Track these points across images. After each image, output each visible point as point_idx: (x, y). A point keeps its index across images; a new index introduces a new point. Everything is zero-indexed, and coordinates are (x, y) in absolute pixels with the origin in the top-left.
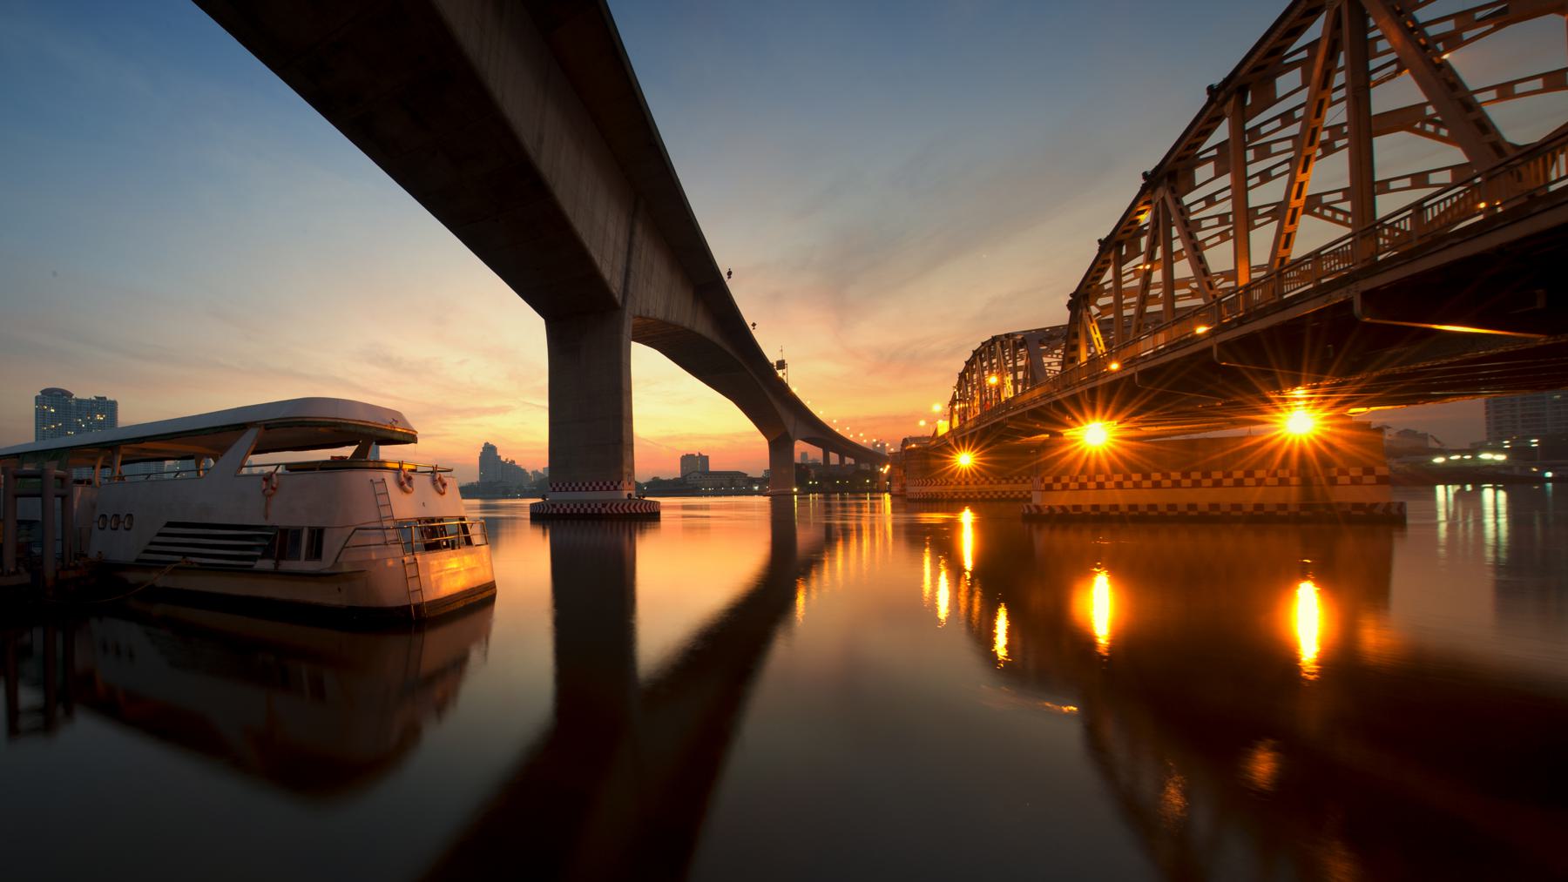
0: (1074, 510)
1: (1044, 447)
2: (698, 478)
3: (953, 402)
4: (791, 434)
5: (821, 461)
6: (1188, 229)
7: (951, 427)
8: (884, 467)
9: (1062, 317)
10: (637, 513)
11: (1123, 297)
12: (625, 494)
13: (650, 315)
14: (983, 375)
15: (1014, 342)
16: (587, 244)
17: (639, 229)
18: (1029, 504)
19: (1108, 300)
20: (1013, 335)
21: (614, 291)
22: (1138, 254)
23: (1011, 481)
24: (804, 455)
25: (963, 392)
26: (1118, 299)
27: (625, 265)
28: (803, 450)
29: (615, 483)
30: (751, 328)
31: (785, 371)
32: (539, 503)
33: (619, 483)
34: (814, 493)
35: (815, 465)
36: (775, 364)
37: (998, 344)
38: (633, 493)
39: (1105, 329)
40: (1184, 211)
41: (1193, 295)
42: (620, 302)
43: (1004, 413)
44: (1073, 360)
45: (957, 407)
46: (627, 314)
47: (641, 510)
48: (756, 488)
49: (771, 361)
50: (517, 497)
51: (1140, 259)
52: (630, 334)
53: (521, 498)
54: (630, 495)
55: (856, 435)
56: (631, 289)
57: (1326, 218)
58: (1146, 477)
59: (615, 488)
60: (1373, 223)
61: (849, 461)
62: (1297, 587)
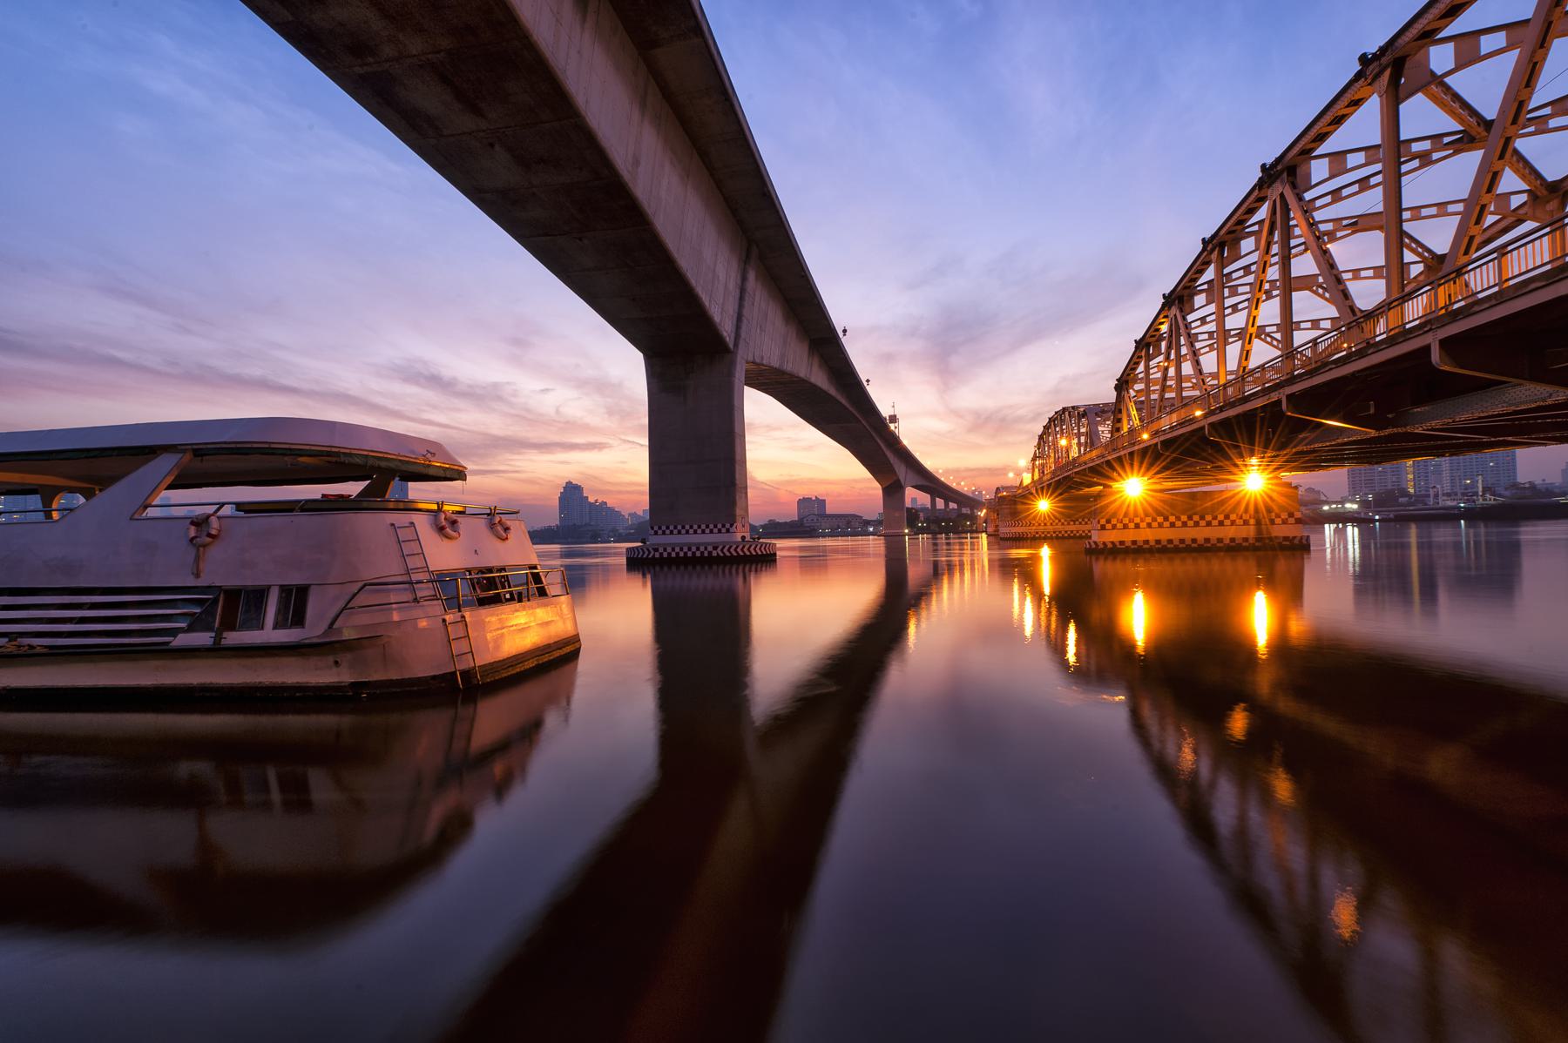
1: (1098, 496)
3: (1034, 459)
5: (929, 506)
6: (1190, 340)
7: (1033, 479)
9: (1110, 396)
15: (1078, 413)
16: (693, 282)
17: (751, 276)
20: (1078, 407)
21: (725, 334)
22: (1160, 354)
23: (1077, 523)
24: (914, 500)
26: (1147, 386)
27: (737, 310)
28: (914, 497)
29: (728, 526)
30: (865, 384)
31: (896, 425)
32: (637, 548)
33: (731, 526)
34: (923, 534)
35: (924, 509)
37: (1067, 413)
39: (1140, 406)
40: (1188, 326)
42: (731, 346)
44: (1118, 430)
45: (1037, 463)
48: (871, 529)
49: (884, 415)
51: (1161, 358)
52: (743, 379)
53: (614, 542)
54: (743, 538)
56: (743, 335)
57: (1267, 343)
58: (1166, 519)
59: (728, 531)
61: (953, 505)
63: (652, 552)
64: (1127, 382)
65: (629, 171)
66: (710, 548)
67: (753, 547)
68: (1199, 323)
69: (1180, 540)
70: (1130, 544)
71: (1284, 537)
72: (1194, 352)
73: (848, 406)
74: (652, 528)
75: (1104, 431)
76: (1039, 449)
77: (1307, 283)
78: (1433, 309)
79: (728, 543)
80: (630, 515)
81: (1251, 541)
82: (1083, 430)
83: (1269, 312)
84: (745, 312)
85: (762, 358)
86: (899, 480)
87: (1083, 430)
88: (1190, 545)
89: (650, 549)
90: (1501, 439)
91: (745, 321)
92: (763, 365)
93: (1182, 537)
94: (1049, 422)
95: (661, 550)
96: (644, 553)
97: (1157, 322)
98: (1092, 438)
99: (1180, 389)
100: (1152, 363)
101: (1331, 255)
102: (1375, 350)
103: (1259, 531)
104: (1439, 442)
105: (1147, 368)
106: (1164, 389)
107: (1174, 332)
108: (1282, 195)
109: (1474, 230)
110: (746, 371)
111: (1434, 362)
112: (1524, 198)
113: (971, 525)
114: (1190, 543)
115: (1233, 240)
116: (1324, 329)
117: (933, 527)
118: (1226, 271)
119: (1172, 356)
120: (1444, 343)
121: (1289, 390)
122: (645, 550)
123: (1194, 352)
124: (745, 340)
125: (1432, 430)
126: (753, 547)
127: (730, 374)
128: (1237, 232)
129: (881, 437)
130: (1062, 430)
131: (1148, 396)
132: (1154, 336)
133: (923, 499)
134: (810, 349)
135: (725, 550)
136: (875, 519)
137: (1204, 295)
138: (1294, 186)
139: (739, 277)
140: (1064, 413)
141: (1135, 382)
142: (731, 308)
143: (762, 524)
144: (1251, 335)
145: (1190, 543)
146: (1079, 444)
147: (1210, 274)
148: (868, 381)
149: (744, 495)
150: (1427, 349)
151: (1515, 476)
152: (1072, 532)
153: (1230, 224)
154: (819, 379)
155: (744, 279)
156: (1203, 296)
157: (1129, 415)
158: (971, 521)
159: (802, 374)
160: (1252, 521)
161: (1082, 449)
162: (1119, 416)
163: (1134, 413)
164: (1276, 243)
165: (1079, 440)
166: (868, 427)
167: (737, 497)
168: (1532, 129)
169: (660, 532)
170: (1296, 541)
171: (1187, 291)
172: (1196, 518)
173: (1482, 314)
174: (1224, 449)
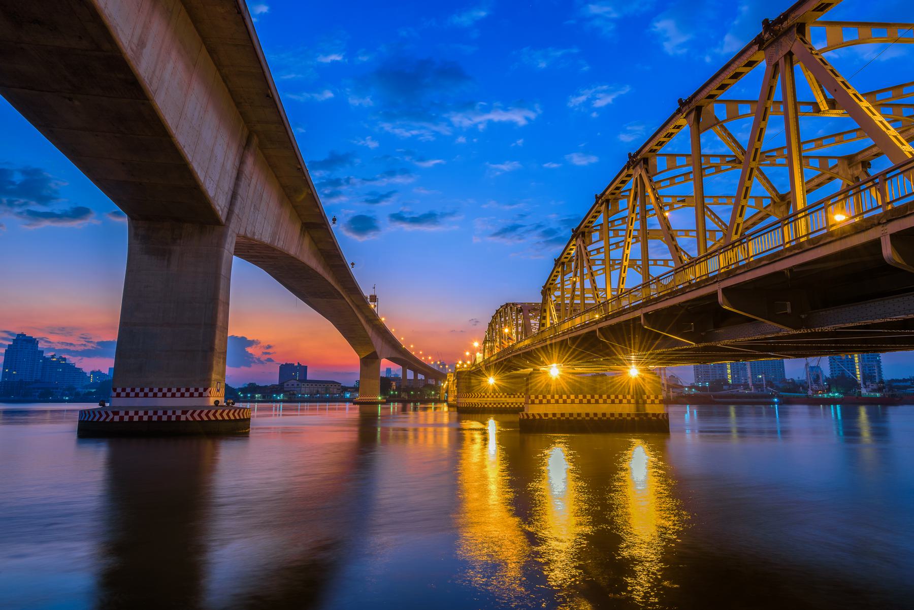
1: (529, 377)
2: (296, 386)
4: (378, 354)
5: (401, 376)
7: (484, 358)
8: (444, 384)
10: (217, 420)
11: (565, 293)
12: (212, 402)
13: (256, 237)
15: (517, 309)
16: (189, 158)
17: (250, 161)
19: (558, 293)
20: (517, 304)
21: (218, 208)
23: (516, 396)
27: (232, 188)
29: (201, 390)
30: (350, 266)
31: (376, 304)
32: (93, 411)
33: (205, 390)
35: (396, 379)
36: (369, 297)
38: (222, 400)
41: (545, 568)
43: (510, 353)
44: (543, 325)
46: (230, 232)
50: (65, 401)
51: (572, 274)
52: (232, 250)
53: (69, 401)
54: (217, 402)
55: (427, 359)
56: (236, 211)
59: (201, 395)
61: (421, 377)
63: (111, 416)
64: (549, 289)
65: (132, 50)
69: (570, 414)
70: (584, 416)
71: (653, 414)
72: (592, 273)
73: (333, 283)
74: (115, 390)
78: (747, 257)
79: (199, 407)
80: (93, 372)
81: (632, 416)
83: (633, 251)
84: (241, 191)
85: (254, 233)
86: (375, 353)
87: (520, 322)
88: (585, 418)
91: (239, 199)
93: (595, 412)
94: (496, 313)
95: (122, 413)
98: (526, 328)
99: (583, 298)
100: (566, 278)
101: (668, 220)
102: (690, 290)
103: (638, 409)
105: (563, 282)
106: (573, 298)
107: (579, 255)
108: (640, 175)
109: (739, 220)
110: (236, 243)
111: (720, 303)
112: (769, 201)
113: (435, 395)
115: (614, 199)
116: (671, 267)
117: (404, 395)
119: (579, 274)
120: (894, 237)
122: (103, 413)
123: (592, 273)
124: (238, 216)
125: (726, 345)
126: (226, 412)
127: (220, 245)
128: (616, 194)
130: (505, 320)
131: (563, 300)
133: (396, 370)
134: (301, 230)
135: (196, 415)
136: (352, 386)
138: (647, 172)
140: (506, 307)
141: (555, 290)
142: (227, 185)
143: (241, 387)
144: (625, 266)
146: (517, 333)
147: (601, 219)
148: (353, 264)
150: (877, 243)
151: (784, 376)
152: (512, 403)
153: (610, 189)
155: (242, 162)
156: (597, 233)
157: (551, 315)
159: (293, 251)
161: (519, 336)
162: (545, 314)
163: (554, 313)
164: (638, 206)
166: (351, 304)
167: (214, 362)
168: (768, 162)
169: (123, 394)
170: (660, 417)
171: (587, 230)
173: (790, 259)
174: (610, 348)
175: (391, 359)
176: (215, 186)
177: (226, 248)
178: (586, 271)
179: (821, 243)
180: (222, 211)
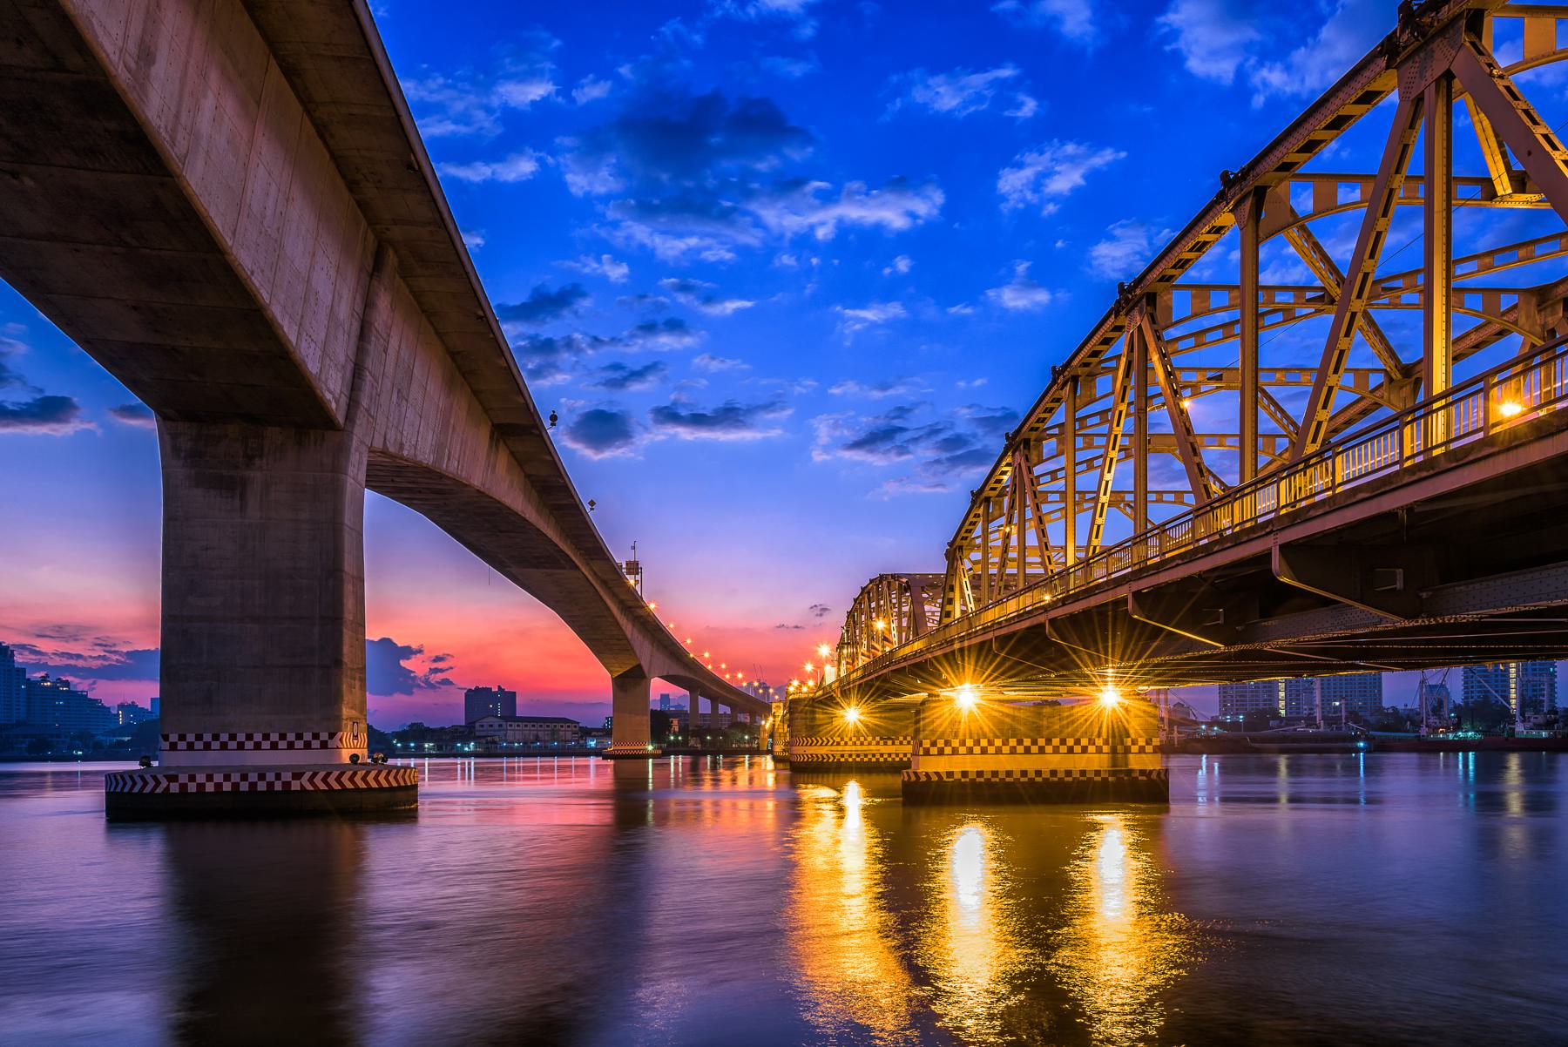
0: (948, 777)
2: (496, 727)
3: (840, 646)
4: (646, 669)
5: (687, 708)
6: (1036, 501)
9: (941, 568)
13: (405, 453)
14: (871, 618)
15: (900, 585)
17: (383, 302)
18: (909, 770)
20: (900, 576)
21: (328, 396)
24: (665, 698)
25: (852, 634)
26: (985, 554)
29: (324, 736)
31: (638, 577)
32: (131, 774)
33: (332, 736)
34: (676, 754)
35: (679, 714)
38: (363, 753)
39: (976, 583)
42: (340, 419)
43: (888, 666)
44: (948, 614)
45: (845, 651)
46: (355, 443)
47: (397, 781)
48: (593, 744)
51: (1003, 520)
52: (362, 477)
54: (354, 758)
55: (734, 677)
59: (324, 745)
60: (1146, 531)
61: (724, 709)
62: (961, 823)
63: (164, 783)
66: (287, 776)
67: (373, 773)
68: (1048, 478)
71: (1140, 771)
72: (1040, 517)
75: (932, 609)
76: (847, 631)
77: (1490, 309)
79: (323, 766)
80: (121, 706)
82: (906, 609)
85: (401, 446)
86: (639, 667)
87: (906, 609)
89: (159, 776)
90: (1350, 662)
92: (402, 458)
93: (1039, 768)
94: (861, 594)
95: (183, 778)
96: (145, 783)
97: (998, 472)
98: (917, 619)
100: (992, 526)
101: (1188, 416)
103: (1114, 763)
104: (1292, 662)
113: (750, 742)
114: (1033, 776)
118: (1079, 414)
121: (1136, 586)
123: (1040, 517)
124: (368, 411)
126: (373, 773)
129: (614, 595)
130: (879, 606)
132: (993, 489)
133: (678, 694)
136: (600, 726)
137: (1054, 440)
138: (1153, 320)
139: (358, 301)
140: (881, 582)
142: (342, 349)
145: (1033, 776)
146: (900, 627)
147: (1060, 415)
148: (592, 503)
149: (358, 684)
150: (1265, 557)
154: (511, 494)
155: (368, 305)
158: (750, 733)
160: (1106, 749)
163: (968, 592)
165: (900, 623)
166: (590, 578)
170: (1154, 776)
171: (1033, 435)
172: (1056, 741)
175: (670, 678)
176: (320, 353)
177: (350, 472)
178: (1029, 514)
179: (1471, 458)
180: (337, 402)
